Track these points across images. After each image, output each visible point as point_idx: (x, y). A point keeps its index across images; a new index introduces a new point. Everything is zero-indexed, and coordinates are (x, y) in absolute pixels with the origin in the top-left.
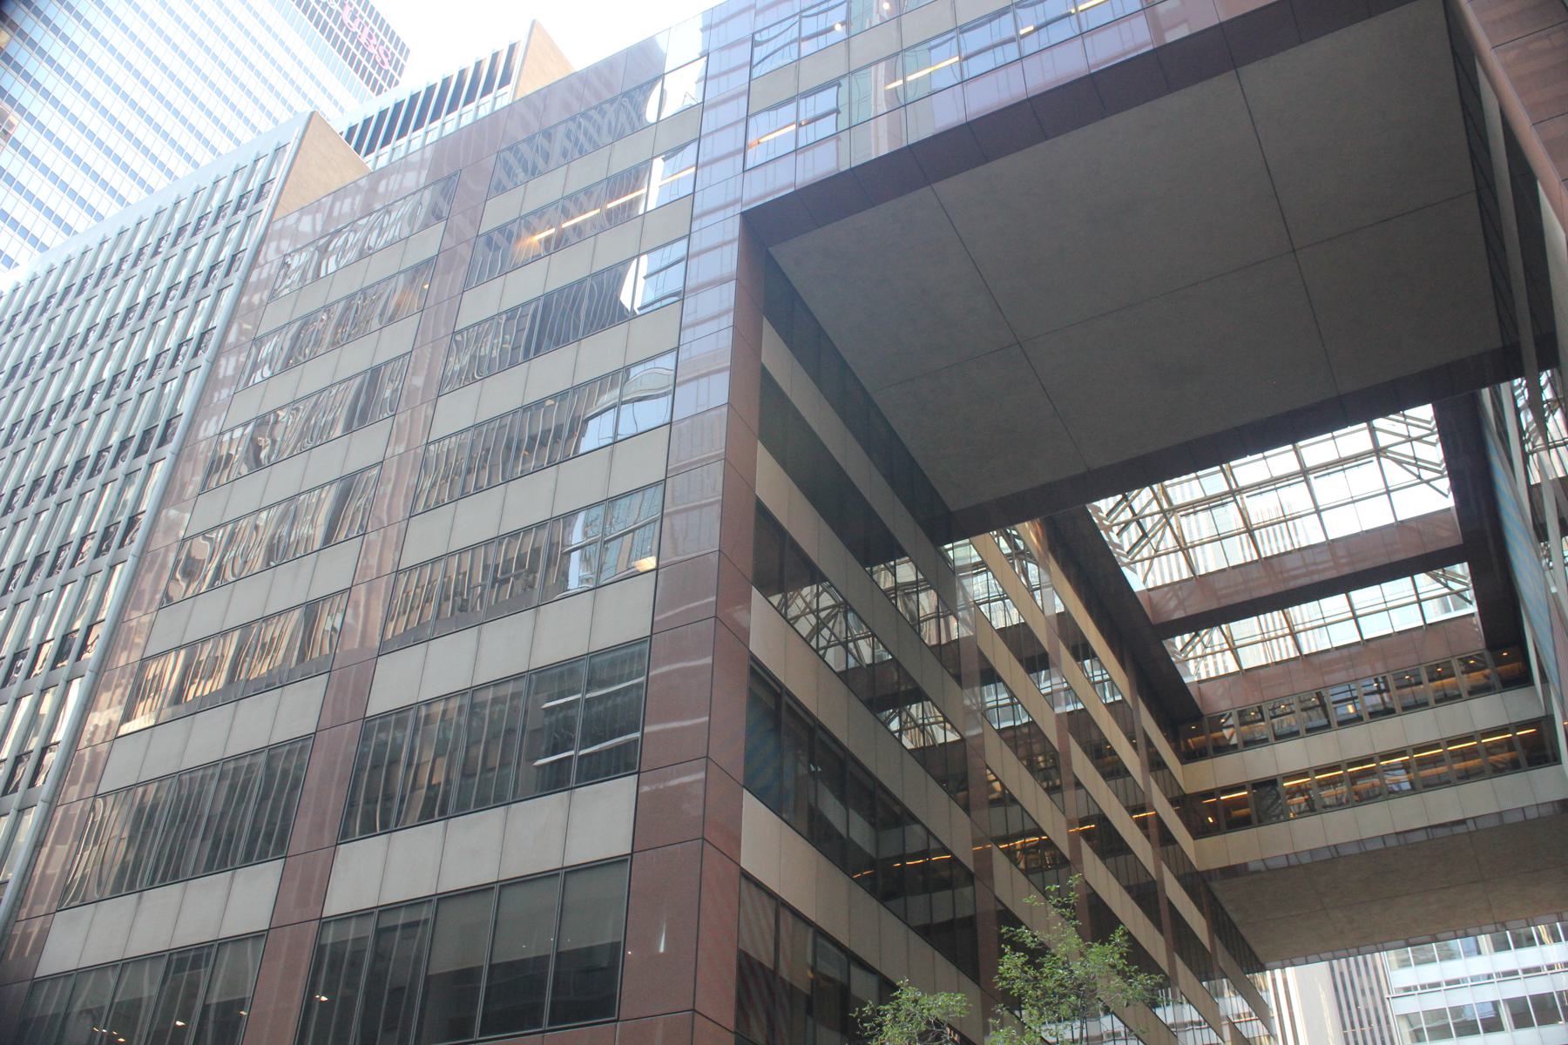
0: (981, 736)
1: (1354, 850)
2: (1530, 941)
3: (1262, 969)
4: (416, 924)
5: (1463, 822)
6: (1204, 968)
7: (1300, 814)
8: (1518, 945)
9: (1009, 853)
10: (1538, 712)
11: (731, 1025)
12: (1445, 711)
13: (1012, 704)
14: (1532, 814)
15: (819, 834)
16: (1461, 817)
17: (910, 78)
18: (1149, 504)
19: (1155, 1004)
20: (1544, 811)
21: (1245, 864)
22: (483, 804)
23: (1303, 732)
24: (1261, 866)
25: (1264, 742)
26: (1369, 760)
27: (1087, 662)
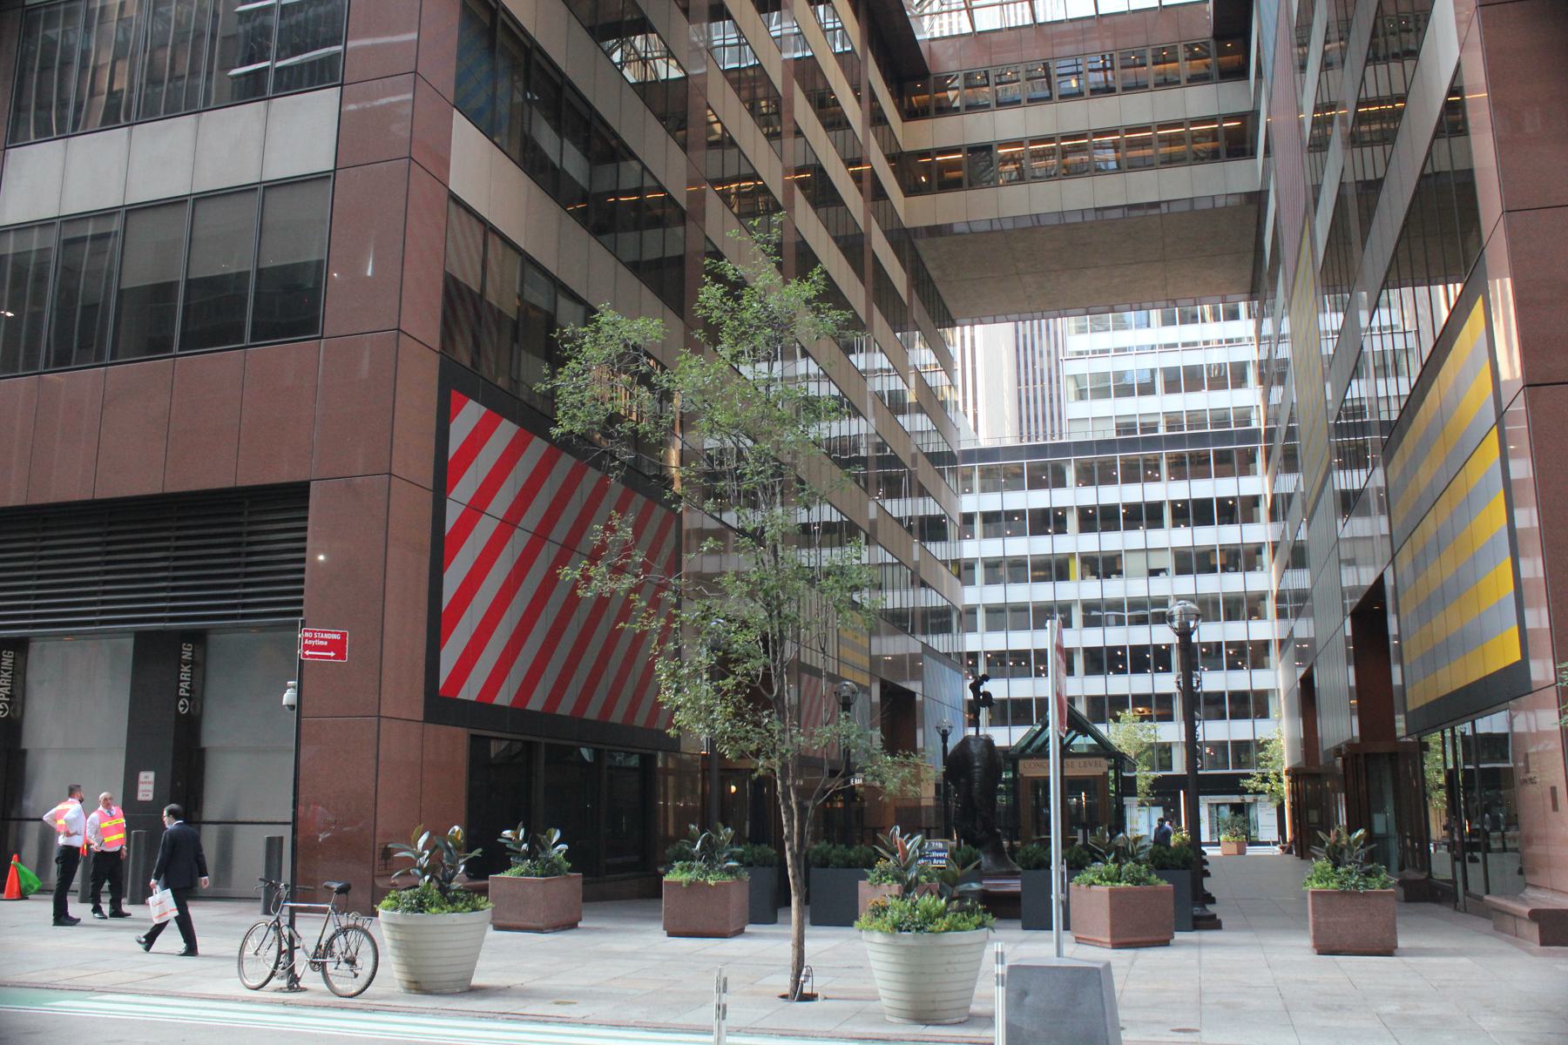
0: (705, 75)
1: (1054, 221)
2: (1194, 319)
3: (953, 324)
4: (106, 236)
5: (1156, 205)
6: (899, 319)
7: (1009, 182)
8: (1183, 322)
9: (724, 196)
10: (1245, 107)
11: (437, 346)
12: (1161, 95)
13: (739, 44)
14: (1220, 203)
15: (534, 163)
16: (1156, 199)
19: (849, 349)
20: (1231, 201)
21: (951, 225)
22: (173, 111)
23: (1024, 102)
24: (964, 228)
25: (986, 107)
26: (1082, 136)
27: (821, 8)
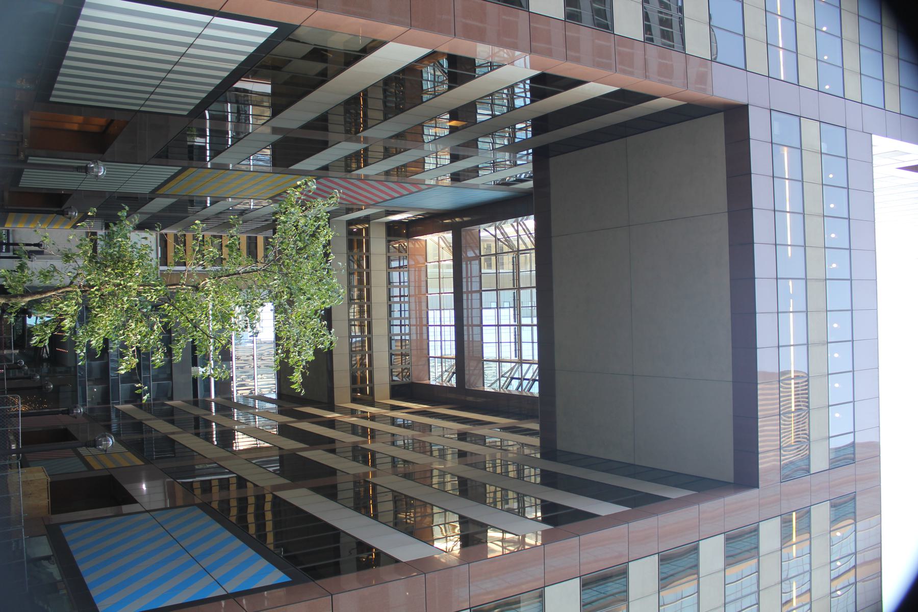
17: (781, 52)
18: (525, 244)
